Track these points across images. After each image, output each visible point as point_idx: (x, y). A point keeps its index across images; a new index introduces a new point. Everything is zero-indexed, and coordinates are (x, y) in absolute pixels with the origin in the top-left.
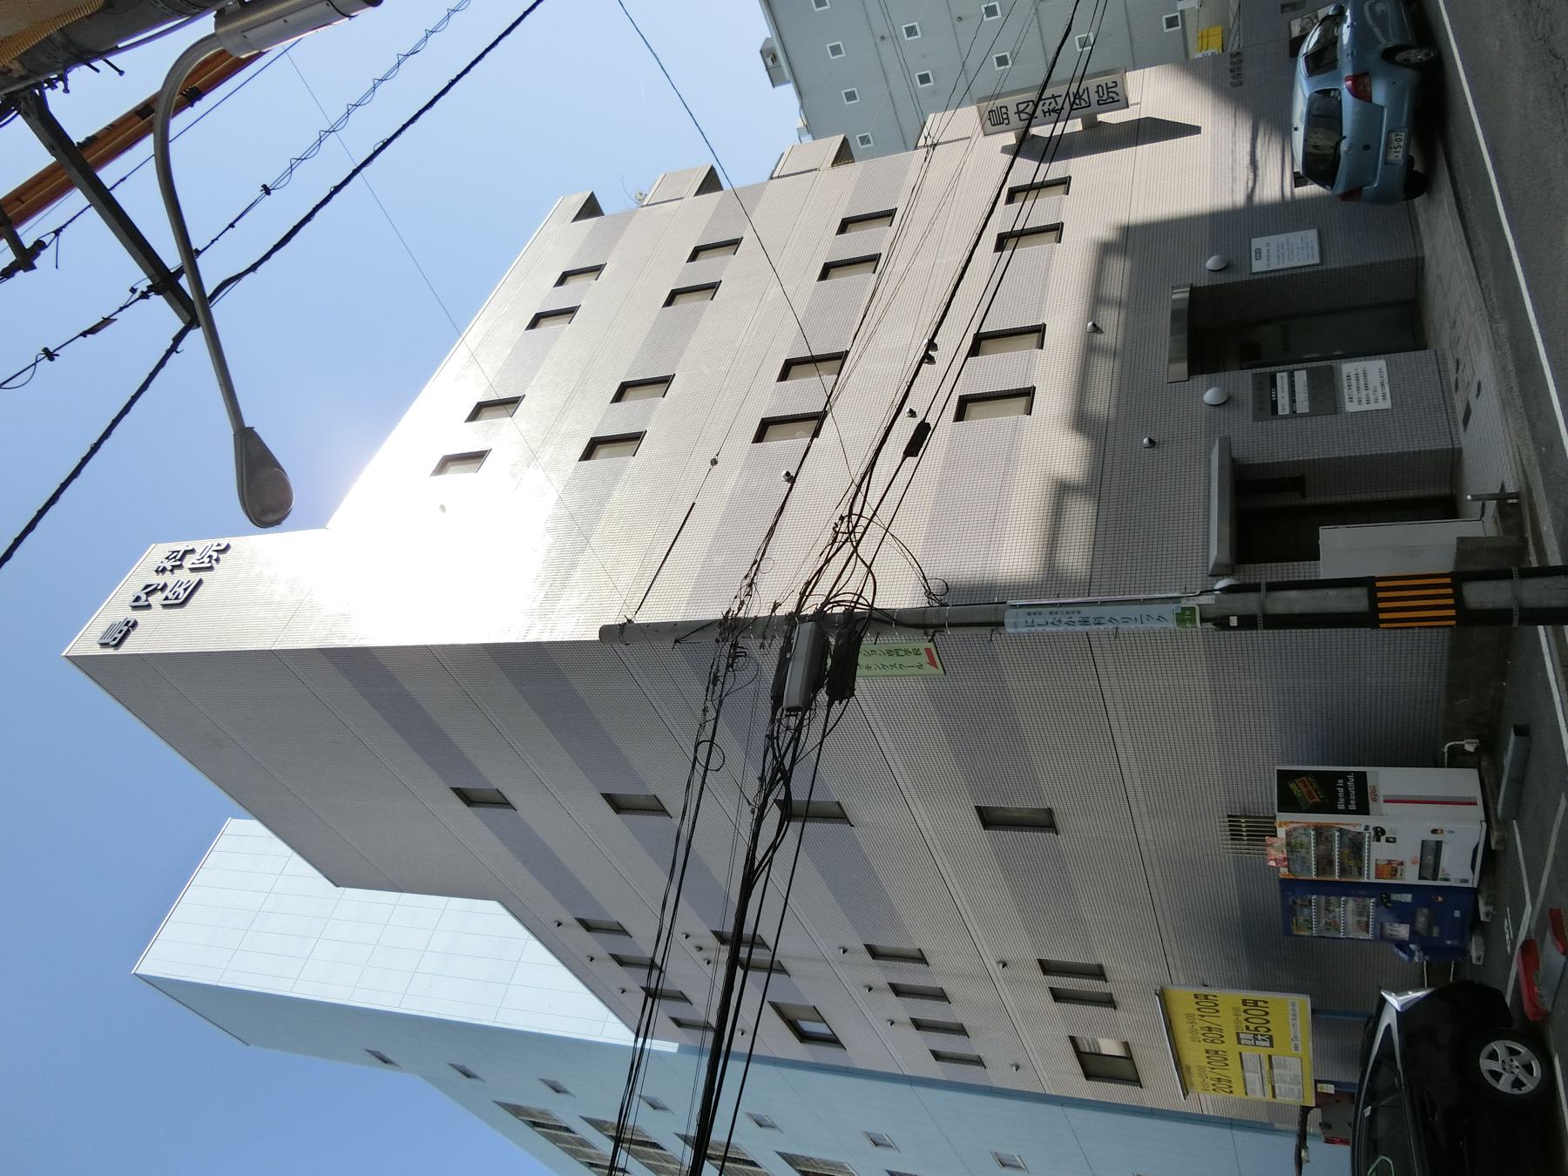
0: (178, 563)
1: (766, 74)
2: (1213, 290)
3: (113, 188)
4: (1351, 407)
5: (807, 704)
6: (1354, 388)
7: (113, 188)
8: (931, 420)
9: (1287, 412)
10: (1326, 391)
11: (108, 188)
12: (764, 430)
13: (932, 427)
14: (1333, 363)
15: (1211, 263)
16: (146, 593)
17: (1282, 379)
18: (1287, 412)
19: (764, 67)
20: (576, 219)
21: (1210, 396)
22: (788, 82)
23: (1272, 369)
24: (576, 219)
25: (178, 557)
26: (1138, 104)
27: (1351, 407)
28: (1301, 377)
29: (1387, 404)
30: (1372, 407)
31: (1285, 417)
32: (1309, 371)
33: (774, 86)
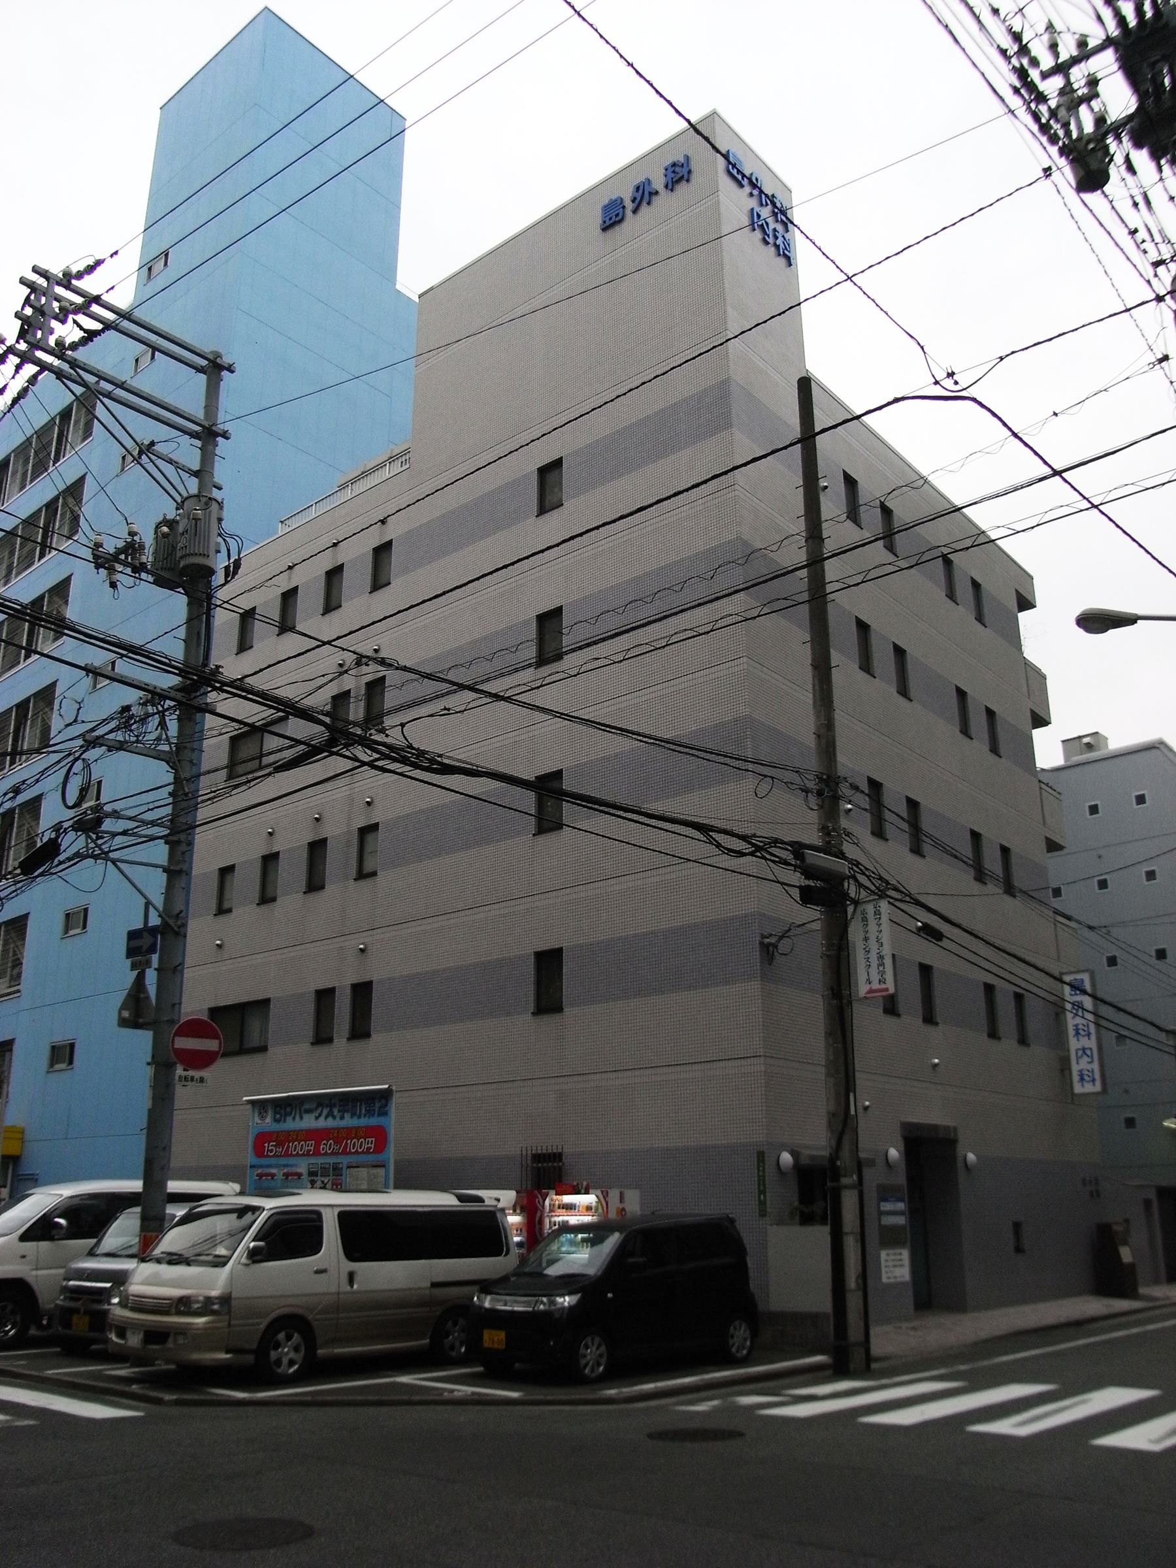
0: (782, 253)
1: (1076, 735)
2: (954, 1158)
3: (1103, 192)
4: (883, 1254)
5: (808, 872)
6: (894, 1257)
7: (1103, 192)
8: (945, 943)
9: (882, 1208)
10: (891, 1238)
11: (1105, 189)
12: (976, 836)
13: (939, 943)
14: (909, 1244)
15: (971, 1157)
16: (762, 224)
17: (901, 1206)
18: (882, 1208)
19: (1081, 734)
20: (1017, 592)
21: (893, 1153)
22: (1067, 757)
23: (906, 1199)
24: (1017, 592)
25: (786, 252)
26: (1072, 1100)
27: (883, 1254)
28: (901, 1220)
29: (884, 1280)
30: (884, 1270)
31: (879, 1208)
32: (903, 1227)
33: (1063, 742)
